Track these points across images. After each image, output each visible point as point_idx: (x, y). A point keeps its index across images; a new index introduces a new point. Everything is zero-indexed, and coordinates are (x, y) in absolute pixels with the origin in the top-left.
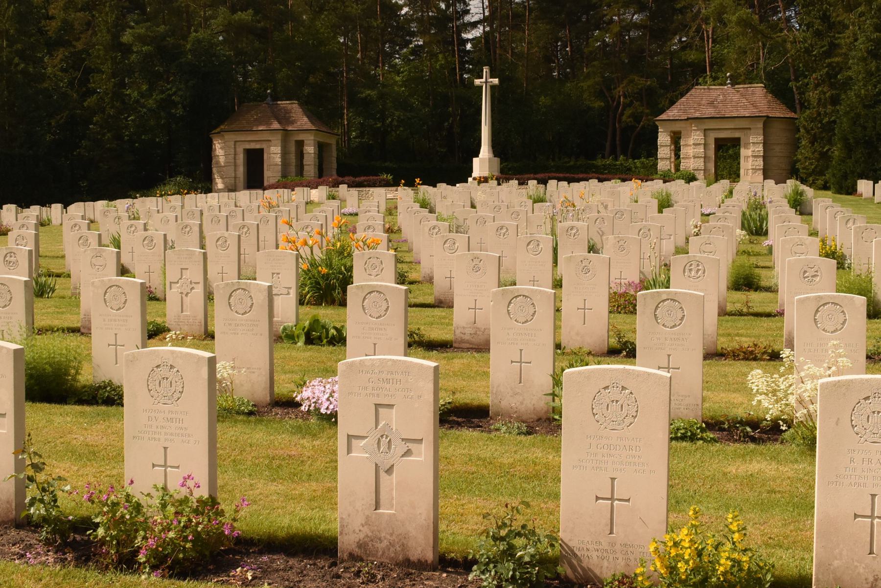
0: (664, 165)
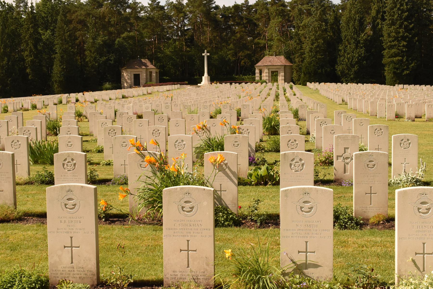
0: (257, 78)
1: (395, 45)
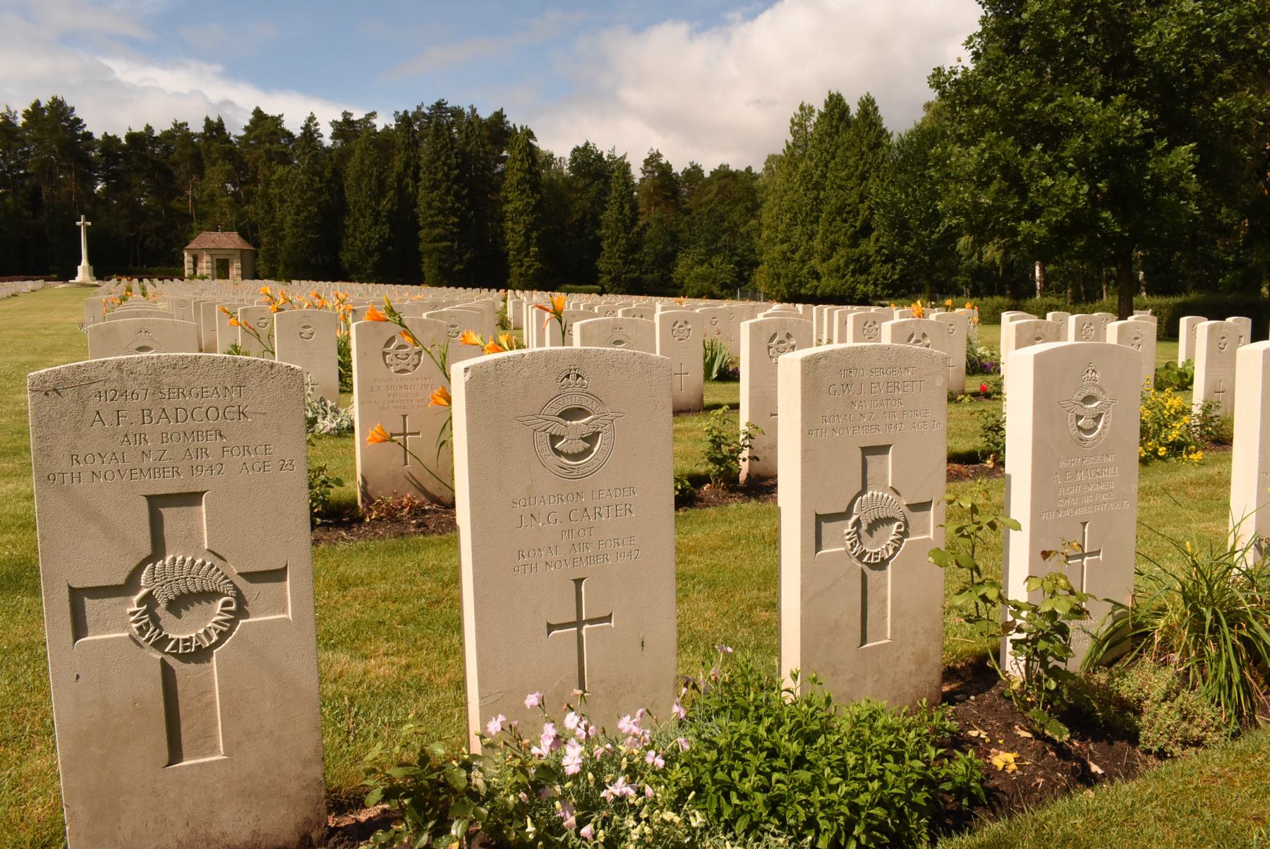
0: (188, 271)
1: (440, 222)
